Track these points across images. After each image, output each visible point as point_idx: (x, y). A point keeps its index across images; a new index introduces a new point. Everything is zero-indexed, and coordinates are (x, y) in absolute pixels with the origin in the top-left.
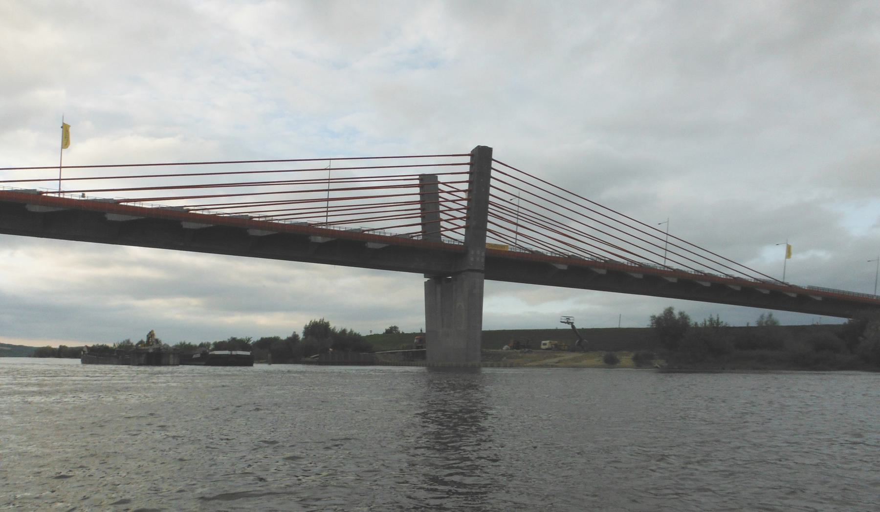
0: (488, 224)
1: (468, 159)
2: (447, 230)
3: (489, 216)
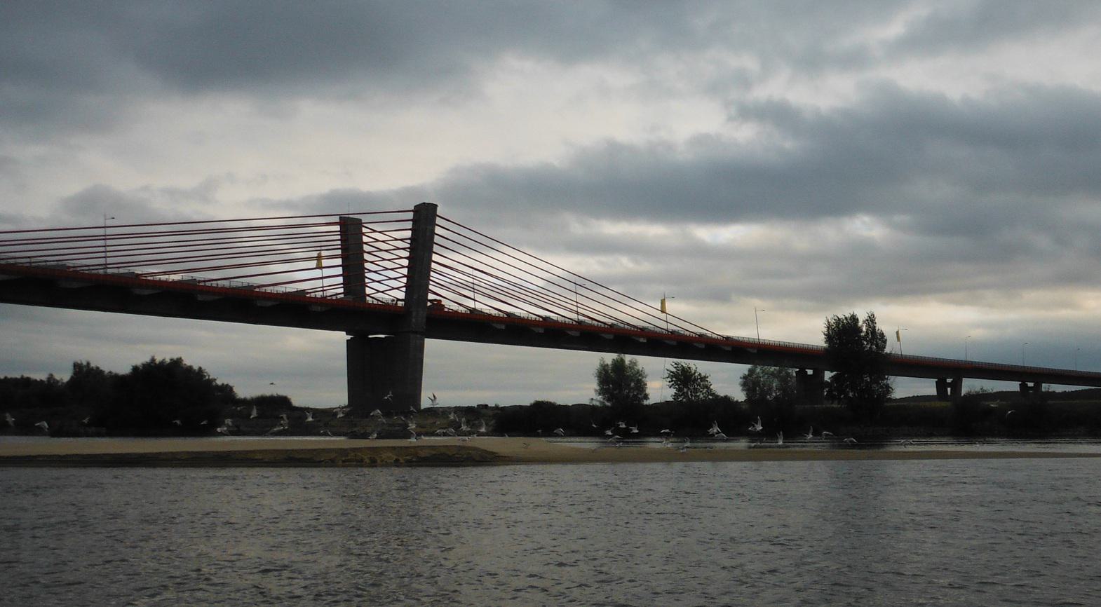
0: (434, 255)
1: (410, 215)
2: (370, 271)
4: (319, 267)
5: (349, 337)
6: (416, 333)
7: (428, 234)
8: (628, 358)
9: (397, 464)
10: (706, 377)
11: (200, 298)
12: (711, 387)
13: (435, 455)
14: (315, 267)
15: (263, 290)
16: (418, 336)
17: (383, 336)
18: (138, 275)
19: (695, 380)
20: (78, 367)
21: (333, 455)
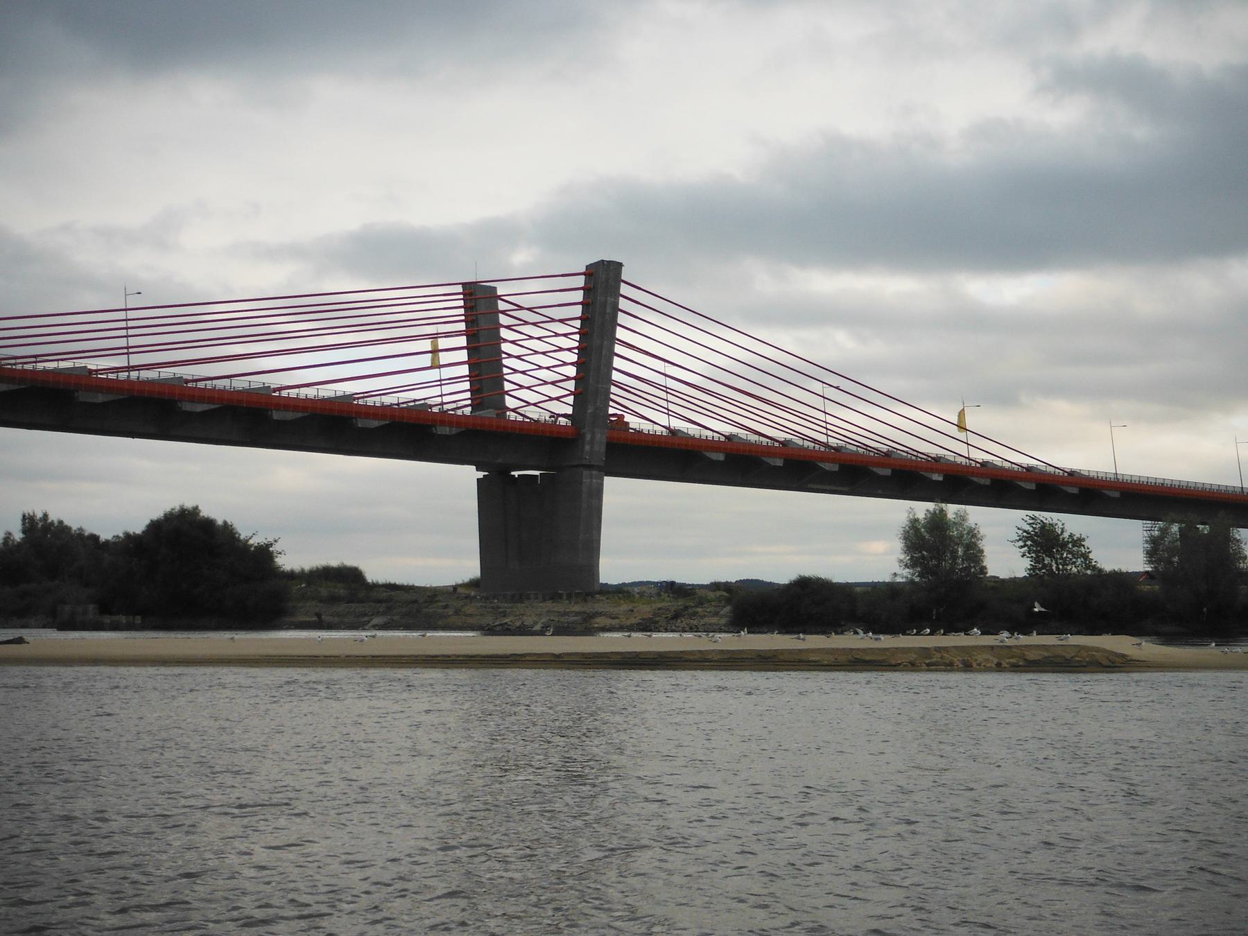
0: (614, 372)
1: (580, 281)
3: (616, 345)
4: (436, 365)
5: (481, 475)
6: (590, 467)
7: (609, 310)
8: (952, 510)
9: (999, 668)
10: (1081, 540)
11: (276, 416)
12: (1091, 556)
13: (1049, 657)
14: (430, 365)
15: (284, 393)
16: (594, 472)
17: (537, 473)
18: (91, 371)
19: (1064, 545)
20: (29, 523)
21: (912, 657)
